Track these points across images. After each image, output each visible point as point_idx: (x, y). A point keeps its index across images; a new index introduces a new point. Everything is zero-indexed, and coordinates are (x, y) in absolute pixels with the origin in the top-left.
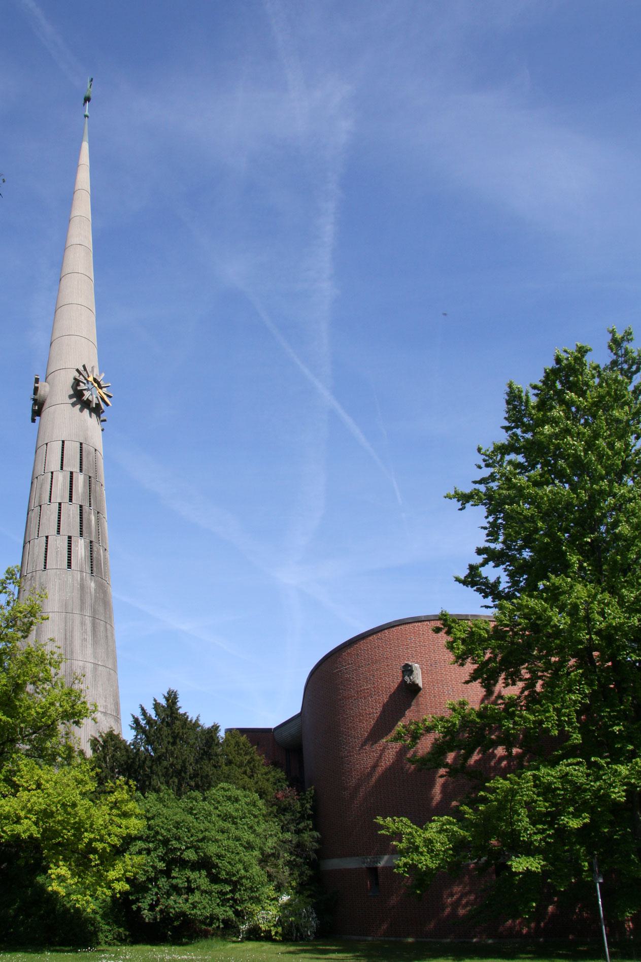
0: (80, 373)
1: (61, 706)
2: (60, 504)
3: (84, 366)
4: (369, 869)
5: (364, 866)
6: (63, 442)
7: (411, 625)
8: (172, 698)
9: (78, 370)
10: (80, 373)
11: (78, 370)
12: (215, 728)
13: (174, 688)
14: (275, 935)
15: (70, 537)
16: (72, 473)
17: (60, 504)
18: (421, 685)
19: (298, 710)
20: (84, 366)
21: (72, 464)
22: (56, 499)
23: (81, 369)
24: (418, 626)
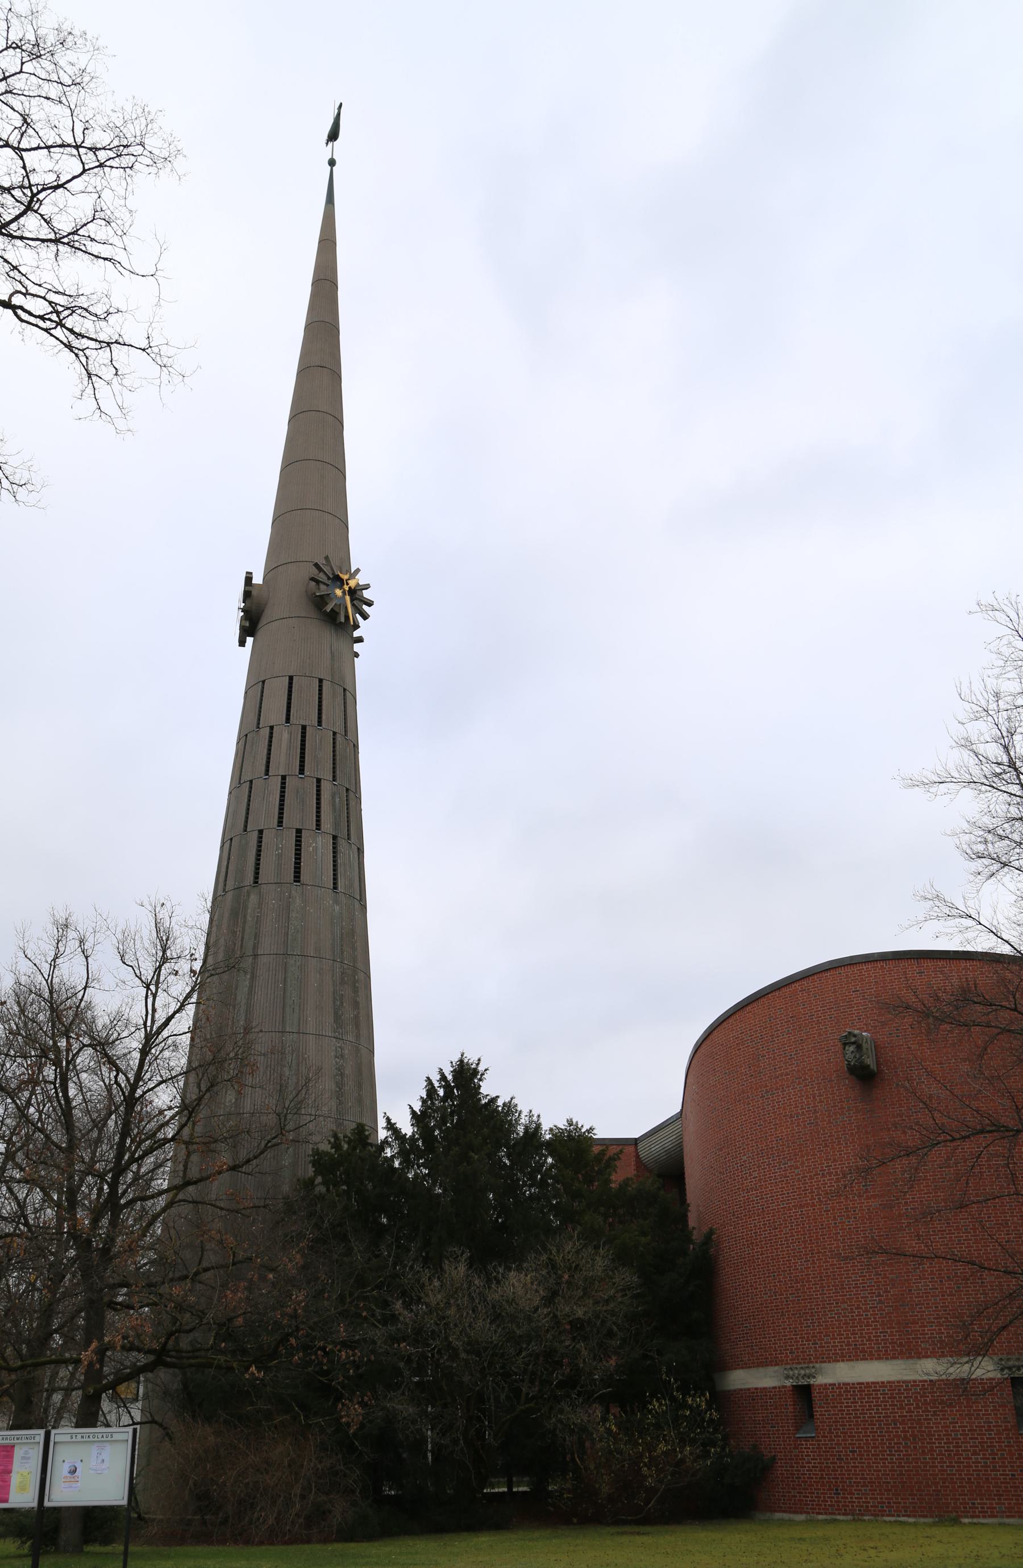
0: (320, 569)
1: (290, 1260)
2: (284, 778)
3: (327, 558)
4: (796, 1388)
5: (788, 1383)
6: (291, 678)
7: (855, 969)
8: (466, 1075)
9: (316, 565)
10: (320, 569)
11: (316, 565)
12: (494, 1100)
13: (471, 1057)
14: (407, 1163)
15: (299, 831)
16: (304, 728)
17: (284, 778)
18: (873, 1066)
19: (678, 1109)
20: (327, 558)
21: (305, 713)
22: (279, 768)
23: (321, 562)
24: (966, 969)
